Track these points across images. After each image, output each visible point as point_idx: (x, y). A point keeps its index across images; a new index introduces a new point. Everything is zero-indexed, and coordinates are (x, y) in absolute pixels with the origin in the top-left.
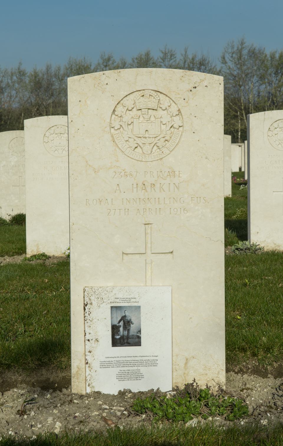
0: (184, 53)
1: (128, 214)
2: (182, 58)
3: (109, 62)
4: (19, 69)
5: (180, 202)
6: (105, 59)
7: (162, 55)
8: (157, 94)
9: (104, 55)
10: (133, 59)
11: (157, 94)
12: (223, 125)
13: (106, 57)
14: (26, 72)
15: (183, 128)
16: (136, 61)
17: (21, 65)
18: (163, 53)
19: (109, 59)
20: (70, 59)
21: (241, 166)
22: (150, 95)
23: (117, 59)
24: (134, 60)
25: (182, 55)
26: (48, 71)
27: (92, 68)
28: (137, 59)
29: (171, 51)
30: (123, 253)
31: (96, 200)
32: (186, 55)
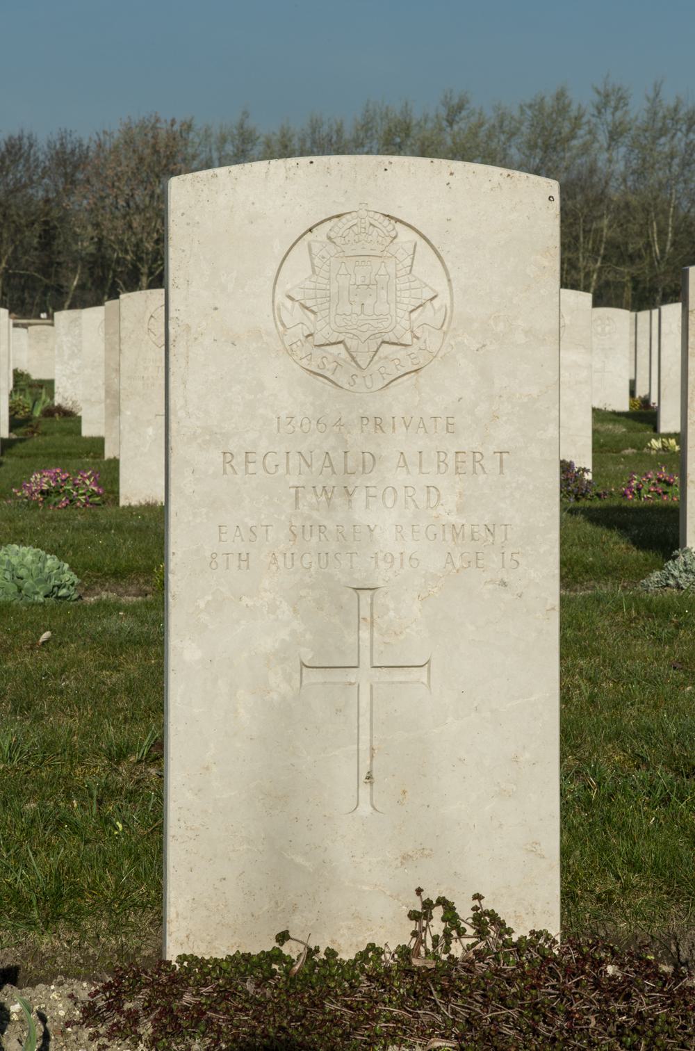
0: (652, 95)
1: (248, 568)
2: (646, 105)
3: (460, 113)
4: (242, 127)
5: (427, 536)
6: (453, 107)
7: (596, 98)
8: (394, 229)
9: (451, 98)
10: (521, 107)
11: (394, 229)
12: (692, 311)
13: (455, 101)
14: (257, 134)
15: (313, 338)
16: (529, 112)
17: (247, 117)
18: (598, 93)
19: (460, 108)
20: (367, 105)
21: (160, 499)
22: (371, 224)
23: (265, 127)
24: (524, 108)
25: (648, 99)
26: (314, 132)
27: (348, 134)
28: (530, 106)
29: (619, 89)
30: (303, 664)
31: (393, 488)
32: (655, 99)
